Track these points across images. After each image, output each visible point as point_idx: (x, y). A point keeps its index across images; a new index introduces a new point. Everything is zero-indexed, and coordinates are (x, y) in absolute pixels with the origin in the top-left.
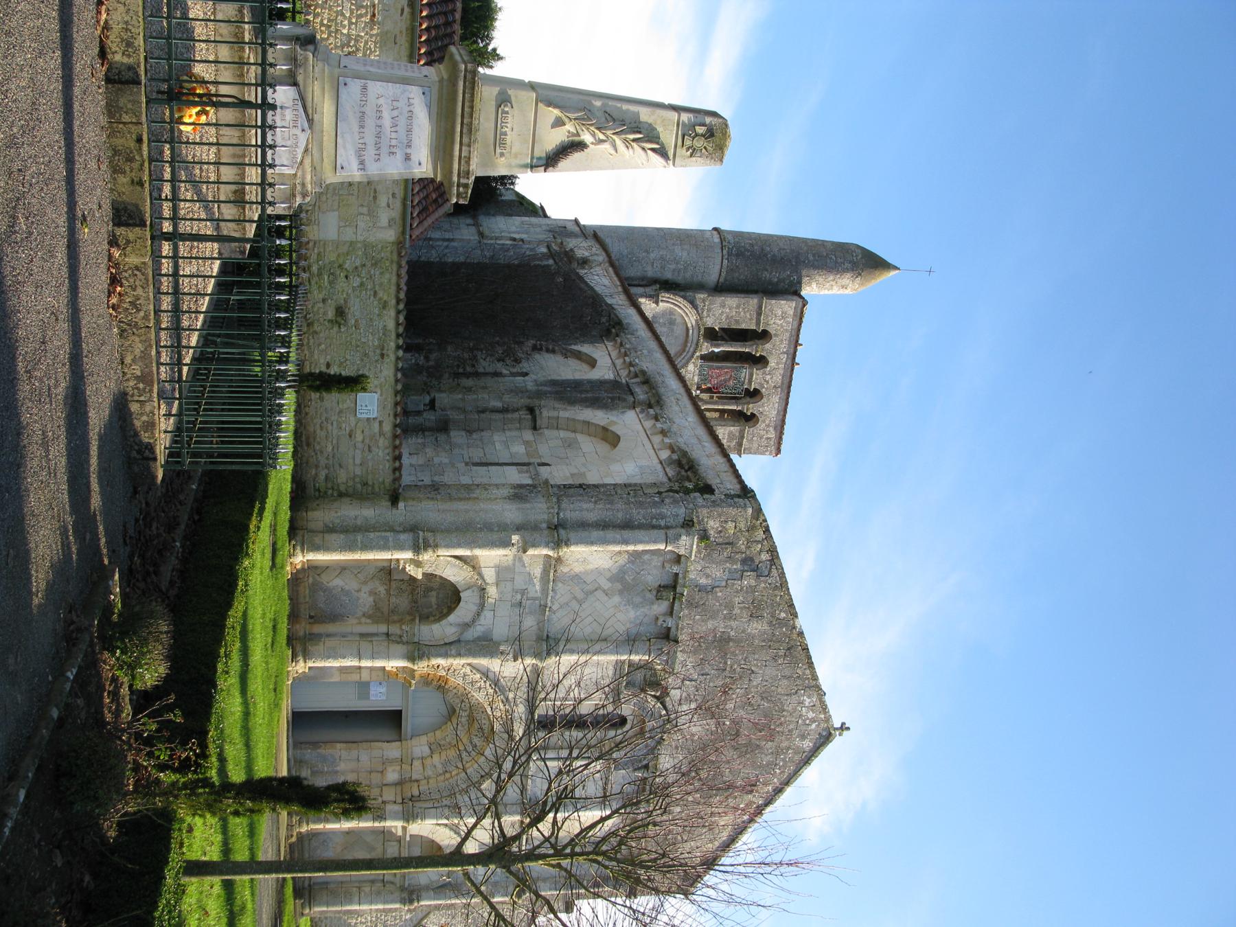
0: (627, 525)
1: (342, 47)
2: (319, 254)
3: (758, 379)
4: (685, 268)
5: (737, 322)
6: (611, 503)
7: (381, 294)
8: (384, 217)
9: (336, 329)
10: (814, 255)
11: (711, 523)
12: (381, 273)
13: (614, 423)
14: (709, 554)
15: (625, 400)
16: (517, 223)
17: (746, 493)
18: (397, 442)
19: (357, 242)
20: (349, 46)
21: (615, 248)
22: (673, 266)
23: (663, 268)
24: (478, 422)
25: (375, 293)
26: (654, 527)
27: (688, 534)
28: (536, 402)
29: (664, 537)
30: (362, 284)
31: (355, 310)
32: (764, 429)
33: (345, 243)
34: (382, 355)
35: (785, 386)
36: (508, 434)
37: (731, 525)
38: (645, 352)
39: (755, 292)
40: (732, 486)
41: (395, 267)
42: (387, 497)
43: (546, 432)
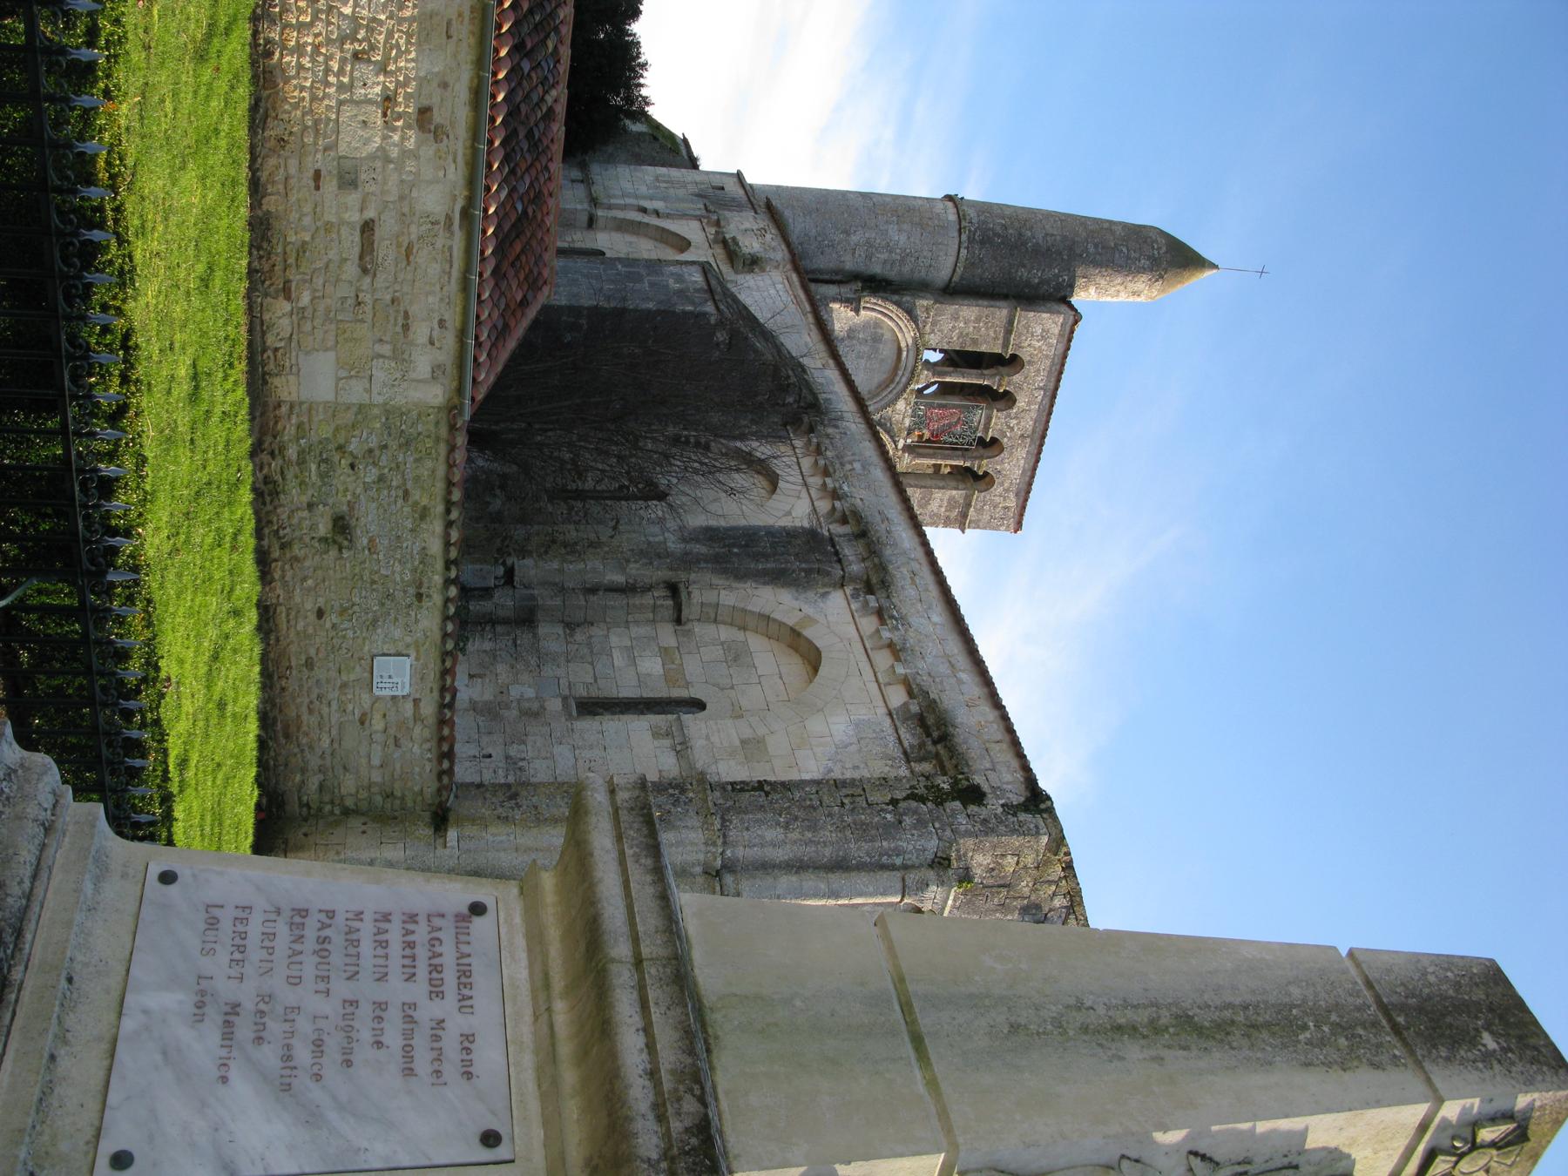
0: (840, 865)
1: (342, 40)
2: (299, 426)
3: (998, 422)
4: (903, 260)
5: (975, 342)
6: (813, 827)
7: (416, 495)
8: (423, 363)
9: (333, 553)
10: (1096, 246)
12: (416, 460)
13: (809, 620)
14: (969, 902)
15: (828, 574)
16: (649, 179)
17: (1036, 800)
18: (448, 664)
19: (371, 405)
20: (354, 40)
21: (799, 226)
22: (884, 256)
23: (869, 257)
24: (584, 609)
25: (406, 494)
26: (883, 867)
28: (683, 576)
29: (899, 886)
30: (381, 479)
31: (368, 520)
32: (1001, 496)
34: (419, 596)
35: (1037, 436)
37: (1010, 861)
38: (857, 466)
39: (1005, 297)
40: (1008, 782)
42: (427, 816)
43: (698, 628)
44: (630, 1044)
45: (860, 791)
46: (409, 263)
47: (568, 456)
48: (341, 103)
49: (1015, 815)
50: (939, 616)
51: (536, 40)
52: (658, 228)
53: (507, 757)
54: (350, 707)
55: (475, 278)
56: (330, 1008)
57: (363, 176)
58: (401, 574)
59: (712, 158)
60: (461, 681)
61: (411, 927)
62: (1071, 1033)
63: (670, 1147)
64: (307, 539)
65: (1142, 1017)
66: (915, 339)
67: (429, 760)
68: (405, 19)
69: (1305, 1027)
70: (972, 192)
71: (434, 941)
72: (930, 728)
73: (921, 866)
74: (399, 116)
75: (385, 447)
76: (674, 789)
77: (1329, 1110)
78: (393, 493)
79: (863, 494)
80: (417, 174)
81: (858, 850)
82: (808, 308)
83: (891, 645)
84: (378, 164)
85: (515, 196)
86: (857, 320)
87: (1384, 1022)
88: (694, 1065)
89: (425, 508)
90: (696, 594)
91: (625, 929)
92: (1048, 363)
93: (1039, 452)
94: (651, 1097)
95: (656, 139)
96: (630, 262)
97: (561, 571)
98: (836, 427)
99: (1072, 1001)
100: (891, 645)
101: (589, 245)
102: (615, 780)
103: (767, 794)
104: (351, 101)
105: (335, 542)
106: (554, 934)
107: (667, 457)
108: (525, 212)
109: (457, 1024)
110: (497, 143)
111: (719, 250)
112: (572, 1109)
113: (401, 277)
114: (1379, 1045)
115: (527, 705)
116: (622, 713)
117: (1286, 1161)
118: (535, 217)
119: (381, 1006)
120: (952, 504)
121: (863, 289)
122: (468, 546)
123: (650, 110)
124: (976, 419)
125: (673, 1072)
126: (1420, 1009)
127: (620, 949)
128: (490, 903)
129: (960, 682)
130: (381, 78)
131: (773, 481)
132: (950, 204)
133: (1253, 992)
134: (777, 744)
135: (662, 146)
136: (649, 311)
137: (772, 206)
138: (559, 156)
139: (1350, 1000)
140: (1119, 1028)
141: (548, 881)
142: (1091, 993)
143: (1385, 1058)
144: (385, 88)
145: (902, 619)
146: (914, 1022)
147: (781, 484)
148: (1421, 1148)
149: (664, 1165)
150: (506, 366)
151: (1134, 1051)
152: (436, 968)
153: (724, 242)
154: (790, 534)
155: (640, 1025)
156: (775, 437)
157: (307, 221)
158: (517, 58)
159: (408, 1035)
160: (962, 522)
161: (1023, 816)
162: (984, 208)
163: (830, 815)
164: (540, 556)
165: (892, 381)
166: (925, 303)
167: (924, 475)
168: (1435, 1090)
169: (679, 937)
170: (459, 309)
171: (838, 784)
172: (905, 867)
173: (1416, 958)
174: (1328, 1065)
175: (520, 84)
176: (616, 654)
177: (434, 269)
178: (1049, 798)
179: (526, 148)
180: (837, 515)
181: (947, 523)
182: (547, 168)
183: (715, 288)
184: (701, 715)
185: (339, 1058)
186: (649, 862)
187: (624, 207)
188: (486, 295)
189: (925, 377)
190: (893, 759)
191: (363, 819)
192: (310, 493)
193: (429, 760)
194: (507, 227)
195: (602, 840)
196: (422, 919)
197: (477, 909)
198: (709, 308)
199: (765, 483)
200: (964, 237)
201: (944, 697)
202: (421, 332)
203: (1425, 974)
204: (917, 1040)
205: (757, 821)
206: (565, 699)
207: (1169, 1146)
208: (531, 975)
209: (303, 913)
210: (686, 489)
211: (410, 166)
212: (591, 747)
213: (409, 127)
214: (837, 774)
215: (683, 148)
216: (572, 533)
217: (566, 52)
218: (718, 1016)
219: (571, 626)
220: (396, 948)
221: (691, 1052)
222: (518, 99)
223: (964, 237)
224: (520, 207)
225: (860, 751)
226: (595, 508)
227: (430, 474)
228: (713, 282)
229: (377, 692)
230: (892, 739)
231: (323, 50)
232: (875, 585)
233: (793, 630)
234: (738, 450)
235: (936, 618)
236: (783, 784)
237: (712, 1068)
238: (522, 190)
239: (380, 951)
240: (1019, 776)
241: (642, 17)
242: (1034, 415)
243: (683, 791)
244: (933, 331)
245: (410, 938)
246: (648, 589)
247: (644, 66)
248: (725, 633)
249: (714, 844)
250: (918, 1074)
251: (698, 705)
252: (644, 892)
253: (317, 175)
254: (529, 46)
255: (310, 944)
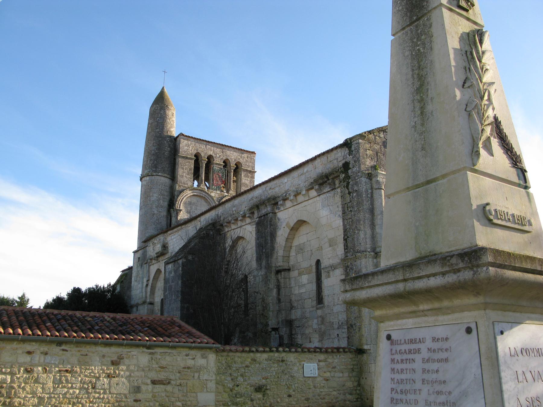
0: (372, 211)
1: (88, 393)
3: (218, 161)
4: (163, 195)
5: (190, 169)
6: (359, 221)
7: (247, 363)
8: (201, 362)
9: (268, 392)
10: (157, 129)
11: (368, 163)
12: (235, 363)
13: (288, 224)
14: (383, 166)
15: (271, 218)
16: (136, 284)
17: (347, 144)
18: (306, 350)
19: (216, 379)
21: (151, 231)
22: (161, 202)
23: (162, 207)
24: (285, 303)
25: (247, 366)
26: (372, 196)
27: (377, 176)
28: (273, 269)
29: (378, 190)
30: (242, 375)
31: (256, 380)
32: (243, 159)
33: (217, 388)
34: (283, 361)
35: (222, 147)
36: (293, 285)
37: (368, 152)
38: (234, 209)
39: (175, 159)
40: (341, 154)
41: (231, 354)
42: (359, 356)
43: (291, 263)
44: (433, 282)
45: (346, 205)
46: (166, 367)
47: (233, 310)
48: (110, 393)
49: (352, 151)
50: (285, 180)
51: (87, 324)
52: (153, 280)
53: (338, 328)
54: (322, 385)
55: (171, 344)
56: (425, 389)
57: (136, 384)
58: (275, 367)
59: (129, 262)
60: (312, 345)
61: (396, 361)
62: (424, 129)
63: (469, 267)
64: (263, 401)
65: (418, 105)
66: (190, 190)
67: (340, 356)
68: (80, 371)
69: (419, 50)
70: (139, 171)
71: (400, 352)
72: (324, 181)
73: (371, 183)
74: (115, 372)
75: (230, 374)
76: (347, 269)
77: (447, 41)
78: (247, 371)
79: (243, 207)
80: (135, 365)
81: (366, 205)
82: (180, 227)
83: (295, 196)
84: (131, 379)
85: (142, 330)
86: (184, 210)
87: (416, 23)
88: (440, 260)
89: (252, 360)
90: (279, 264)
91: (394, 285)
92: (197, 144)
93: (228, 146)
94: (452, 274)
95: (122, 282)
96: (165, 290)
97: (273, 311)
98: (221, 217)
99: (413, 129)
100: (295, 196)
101: (159, 304)
102: (342, 290)
103: (348, 237)
104: (109, 389)
105: (264, 391)
106: (397, 310)
107: (232, 275)
108: (148, 327)
109: (429, 343)
110: (124, 337)
111: (160, 259)
112: (457, 302)
113: (171, 370)
114: (424, 25)
115: (320, 322)
116: (321, 289)
117: (464, 55)
118: (150, 323)
119: (424, 371)
120: (246, 176)
121: (173, 208)
122: (265, 344)
123: (112, 284)
124: (217, 168)
125: (442, 267)
126: (411, 11)
127: (401, 287)
128: (386, 333)
129: (307, 172)
130: (101, 379)
131: (240, 238)
132: (143, 179)
133: (408, 68)
134: (331, 234)
135: (125, 279)
136: (182, 282)
137: (145, 241)
138: (128, 315)
139: (409, 35)
140: (422, 113)
141: (378, 313)
142: (410, 123)
143: (428, 23)
144: (105, 377)
145: (286, 192)
146: (422, 183)
147: (241, 235)
148: (458, 10)
149: (475, 269)
150: (202, 332)
151: (429, 107)
152: (410, 352)
153: (158, 257)
154: (258, 231)
155: (427, 279)
156: (224, 238)
157: (152, 404)
158: (94, 331)
159: (434, 361)
160: (253, 172)
161: (353, 148)
162: (144, 167)
163: (354, 215)
164: (268, 319)
165: (204, 198)
166: (177, 187)
167: (237, 186)
168: (438, 6)
169: (396, 266)
170: (182, 349)
171: (344, 213)
172: (372, 188)
173: (394, 14)
174: (431, 42)
175: (103, 330)
176: (301, 291)
177: (168, 358)
178: (346, 140)
179: (125, 327)
180: (251, 215)
181: (253, 177)
182: (132, 320)
183: (173, 260)
184: (321, 261)
185: (443, 385)
186: (370, 277)
187: (146, 292)
188: (177, 340)
189: (203, 186)
190: (334, 194)
191: (361, 379)
192: (247, 401)
193: (340, 356)
194: (153, 333)
195: (363, 294)
196: (393, 357)
197: (389, 337)
198: (180, 262)
199: (241, 241)
200: (155, 174)
201: (312, 177)
202: (190, 363)
203: (399, 10)
204: (429, 182)
205: (357, 240)
206: (317, 309)
207: (461, 94)
208: (410, 318)
209: (392, 399)
210: (243, 268)
211: (132, 368)
212: (334, 299)
213: (118, 369)
214: (340, 213)
215: (125, 272)
216: (259, 308)
217: (92, 314)
218: (423, 252)
219: (292, 307)
220: (404, 366)
221: (435, 261)
222: (108, 330)
223: (155, 174)
224: (146, 329)
225: (332, 205)
226: (251, 300)
227: (240, 358)
228: (171, 260)
229: (317, 375)
230: (328, 195)
231: (92, 400)
232: (275, 202)
233: (291, 230)
234: (230, 251)
235: (286, 181)
236: (344, 232)
237: (441, 253)
238: (140, 328)
239: (405, 372)
240: (339, 150)
241: (80, 287)
242: (215, 148)
243: (348, 266)
244: (187, 184)
245: (400, 361)
246: (278, 281)
247: (97, 286)
248: (293, 253)
249: (366, 255)
250: (440, 182)
251: (318, 262)
252: (380, 279)
253: (136, 401)
254: (90, 327)
255: (403, 397)
